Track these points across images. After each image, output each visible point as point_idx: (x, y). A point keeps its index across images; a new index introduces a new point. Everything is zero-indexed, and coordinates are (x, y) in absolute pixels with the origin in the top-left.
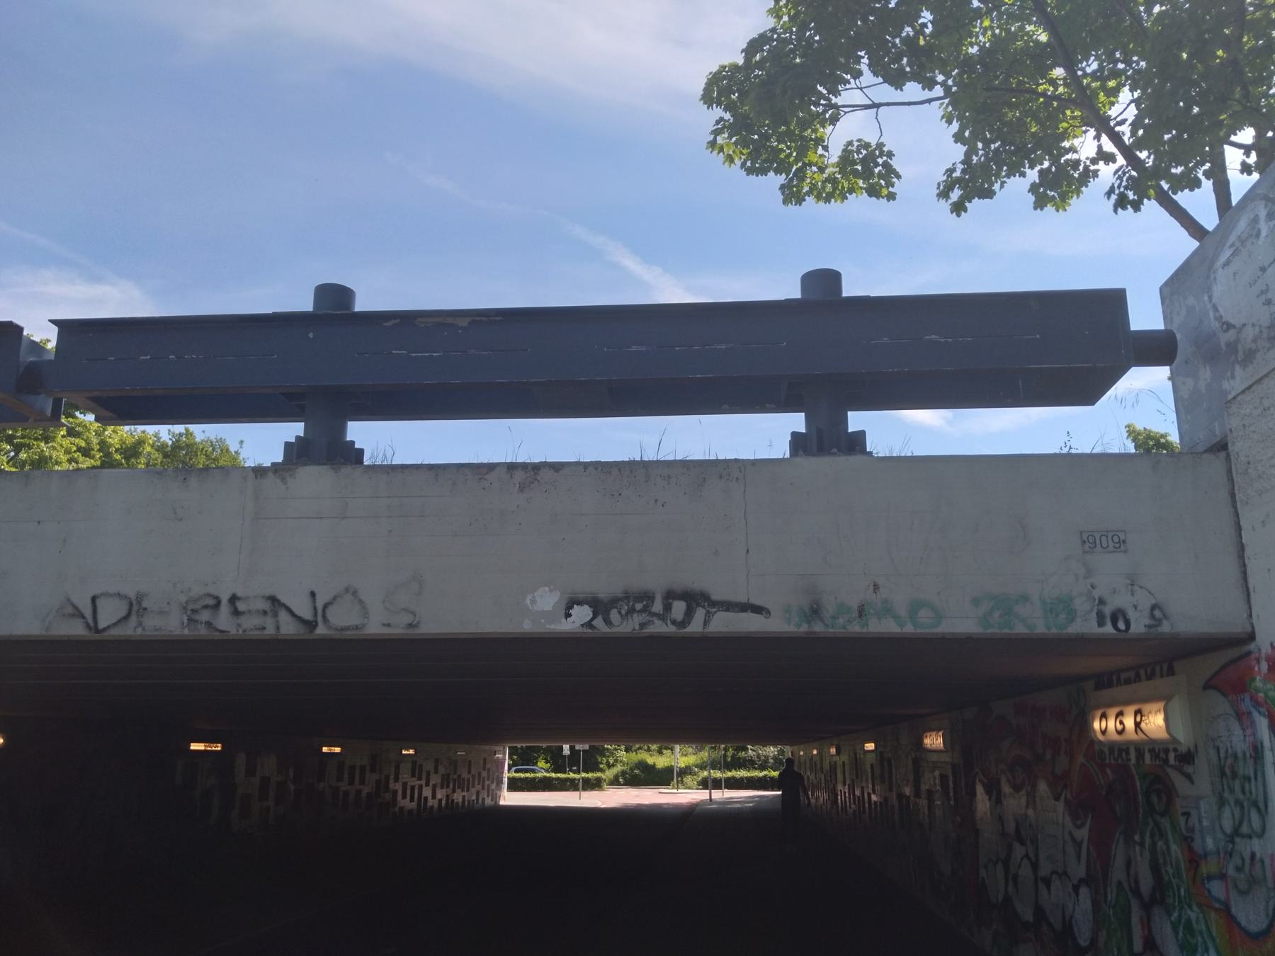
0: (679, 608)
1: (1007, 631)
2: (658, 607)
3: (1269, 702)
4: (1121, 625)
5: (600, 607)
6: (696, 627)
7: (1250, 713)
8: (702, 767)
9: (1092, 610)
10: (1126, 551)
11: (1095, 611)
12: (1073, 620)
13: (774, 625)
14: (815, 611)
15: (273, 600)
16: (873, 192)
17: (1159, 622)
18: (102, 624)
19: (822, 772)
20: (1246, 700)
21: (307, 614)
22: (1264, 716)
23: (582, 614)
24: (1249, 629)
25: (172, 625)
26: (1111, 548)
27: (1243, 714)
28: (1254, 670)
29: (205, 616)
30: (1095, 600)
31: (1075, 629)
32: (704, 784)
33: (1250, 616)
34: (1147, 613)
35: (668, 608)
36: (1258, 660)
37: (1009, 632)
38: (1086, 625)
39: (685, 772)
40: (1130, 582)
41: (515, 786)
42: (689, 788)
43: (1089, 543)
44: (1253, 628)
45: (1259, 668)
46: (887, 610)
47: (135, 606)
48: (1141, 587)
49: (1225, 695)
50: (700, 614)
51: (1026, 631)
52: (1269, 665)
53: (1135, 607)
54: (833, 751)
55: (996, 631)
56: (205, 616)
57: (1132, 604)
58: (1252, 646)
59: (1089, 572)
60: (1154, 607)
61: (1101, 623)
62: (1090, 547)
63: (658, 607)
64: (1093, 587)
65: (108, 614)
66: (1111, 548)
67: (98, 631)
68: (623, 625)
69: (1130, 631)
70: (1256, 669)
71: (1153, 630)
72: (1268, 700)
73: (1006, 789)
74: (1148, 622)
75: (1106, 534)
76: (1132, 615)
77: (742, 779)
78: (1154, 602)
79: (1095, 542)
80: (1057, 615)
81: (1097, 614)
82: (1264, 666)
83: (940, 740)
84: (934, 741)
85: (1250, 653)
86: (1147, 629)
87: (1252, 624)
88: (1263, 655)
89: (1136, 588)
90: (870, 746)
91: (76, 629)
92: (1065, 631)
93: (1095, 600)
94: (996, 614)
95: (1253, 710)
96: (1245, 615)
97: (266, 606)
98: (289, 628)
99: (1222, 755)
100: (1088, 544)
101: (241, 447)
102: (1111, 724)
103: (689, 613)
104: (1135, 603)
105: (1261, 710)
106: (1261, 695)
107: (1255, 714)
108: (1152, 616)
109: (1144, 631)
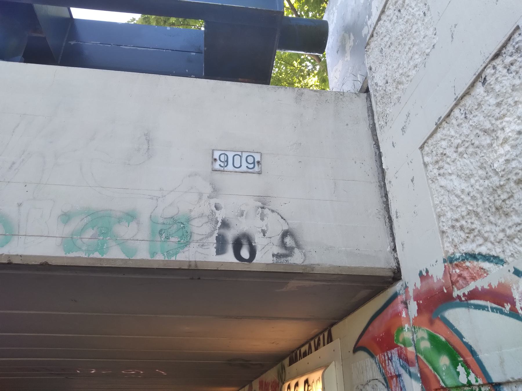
1: (97, 255)
3: (422, 357)
4: (245, 253)
7: (399, 376)
9: (211, 235)
10: (259, 173)
11: (215, 235)
12: (187, 244)
17: (289, 251)
20: (393, 359)
22: (416, 379)
24: (394, 265)
26: (244, 168)
27: (392, 377)
28: (401, 316)
30: (217, 222)
33: (394, 249)
34: (277, 239)
36: (405, 304)
37: (99, 256)
40: (260, 204)
43: (221, 161)
44: (399, 264)
45: (407, 314)
48: (273, 211)
49: (372, 356)
51: (122, 256)
52: (418, 304)
53: (264, 232)
55: (83, 255)
57: (260, 230)
58: (398, 287)
59: (216, 191)
60: (285, 234)
61: (221, 250)
62: (220, 165)
64: (217, 207)
66: (244, 168)
69: (254, 261)
70: (404, 315)
71: (283, 260)
72: (420, 355)
74: (277, 250)
75: (240, 153)
76: (259, 241)
78: (286, 228)
79: (227, 161)
80: (167, 238)
81: (217, 238)
82: (413, 307)
85: (395, 296)
86: (275, 258)
87: (397, 259)
88: (411, 293)
89: (266, 211)
92: (173, 258)
93: (217, 222)
94: (90, 233)
95: (402, 371)
96: (389, 249)
99: (395, 368)
100: (218, 162)
104: (264, 228)
105: (413, 370)
106: (411, 349)
107: (405, 377)
108: (283, 244)
109: (272, 262)
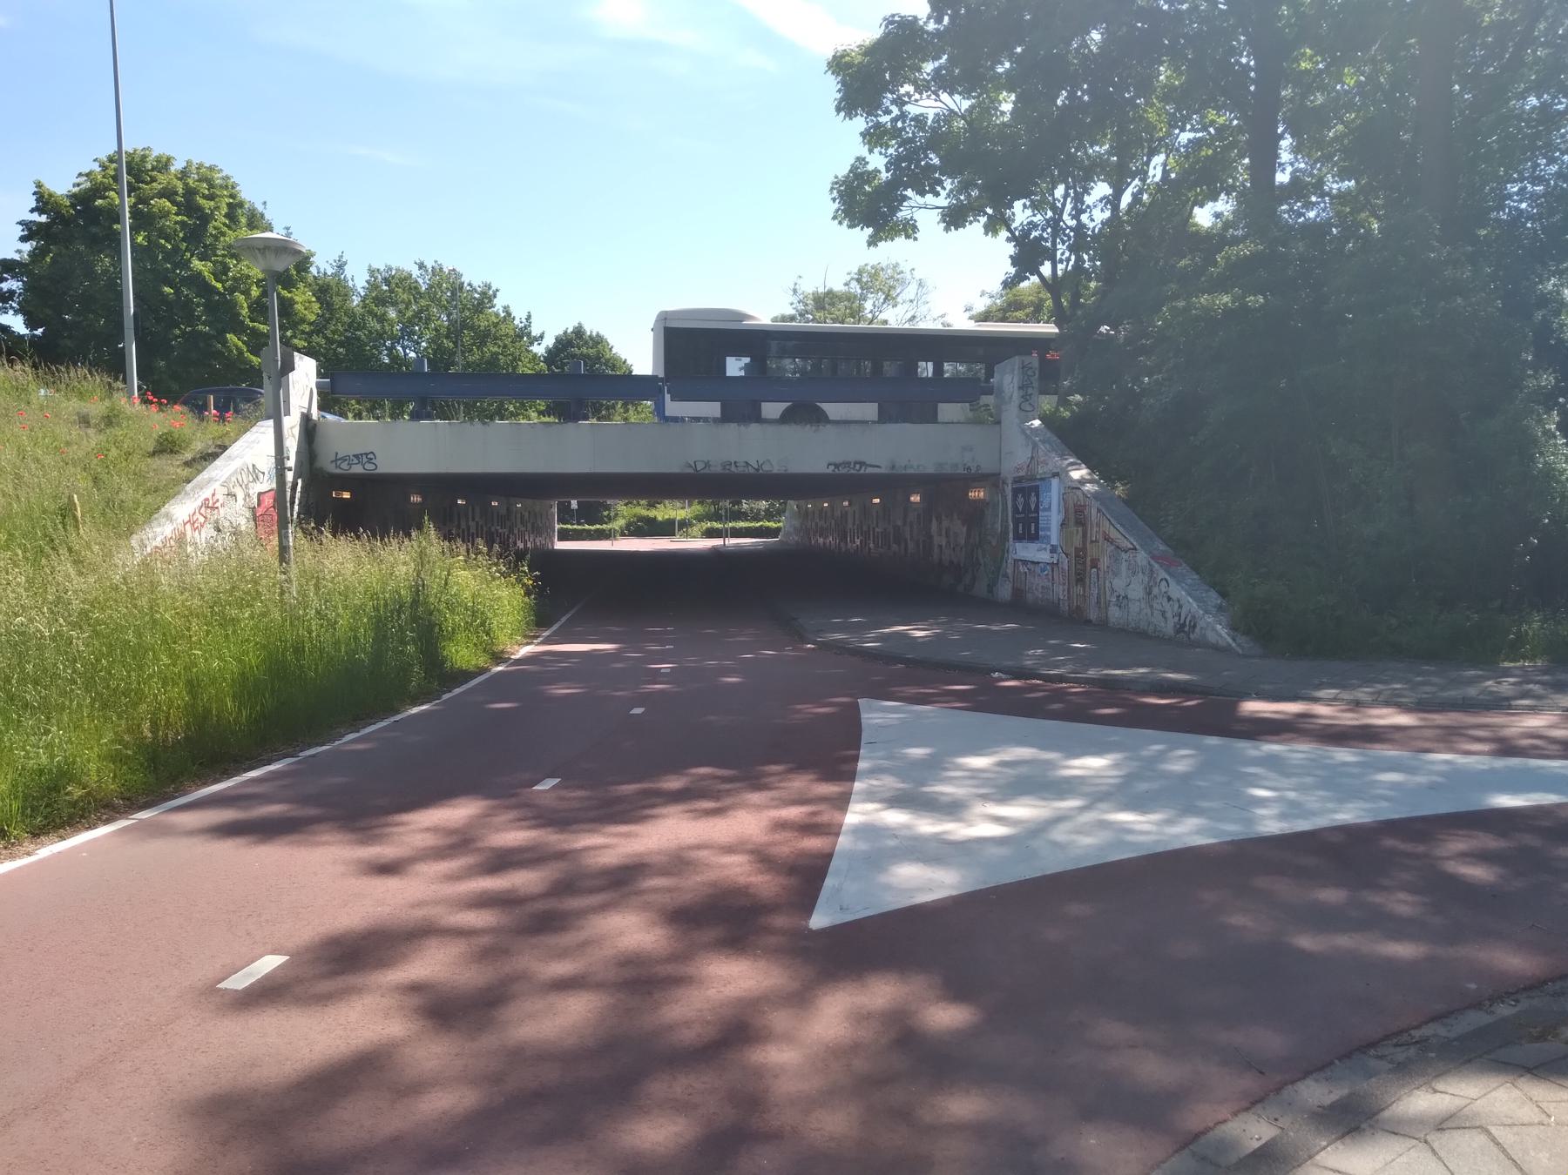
0: (858, 467)
2: (852, 466)
5: (837, 466)
6: (862, 471)
8: (700, 519)
13: (882, 471)
14: (893, 467)
15: (746, 463)
16: (908, 237)
17: (978, 470)
18: (698, 469)
19: (833, 519)
21: (756, 467)
23: (832, 468)
25: (719, 470)
29: (728, 467)
31: (959, 471)
32: (710, 534)
35: (855, 466)
38: (961, 471)
39: (684, 524)
41: (564, 536)
42: (694, 537)
46: (912, 467)
47: (707, 464)
50: (863, 468)
54: (846, 503)
56: (728, 467)
63: (852, 466)
65: (700, 466)
67: (697, 471)
68: (843, 471)
73: (943, 517)
77: (741, 528)
83: (919, 498)
84: (915, 498)
90: (877, 501)
91: (690, 471)
97: (745, 464)
98: (752, 471)
101: (265, 208)
102: (973, 494)
103: (861, 468)
